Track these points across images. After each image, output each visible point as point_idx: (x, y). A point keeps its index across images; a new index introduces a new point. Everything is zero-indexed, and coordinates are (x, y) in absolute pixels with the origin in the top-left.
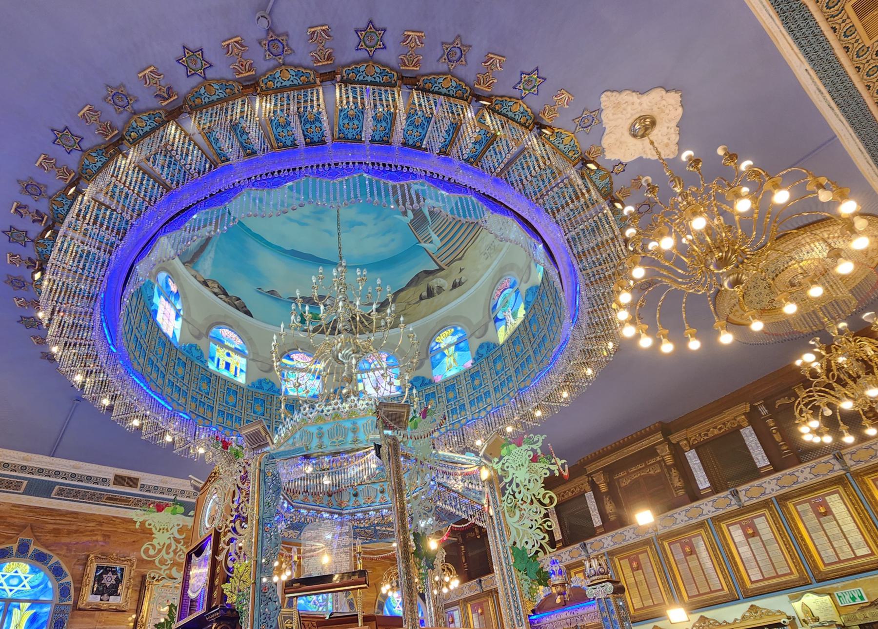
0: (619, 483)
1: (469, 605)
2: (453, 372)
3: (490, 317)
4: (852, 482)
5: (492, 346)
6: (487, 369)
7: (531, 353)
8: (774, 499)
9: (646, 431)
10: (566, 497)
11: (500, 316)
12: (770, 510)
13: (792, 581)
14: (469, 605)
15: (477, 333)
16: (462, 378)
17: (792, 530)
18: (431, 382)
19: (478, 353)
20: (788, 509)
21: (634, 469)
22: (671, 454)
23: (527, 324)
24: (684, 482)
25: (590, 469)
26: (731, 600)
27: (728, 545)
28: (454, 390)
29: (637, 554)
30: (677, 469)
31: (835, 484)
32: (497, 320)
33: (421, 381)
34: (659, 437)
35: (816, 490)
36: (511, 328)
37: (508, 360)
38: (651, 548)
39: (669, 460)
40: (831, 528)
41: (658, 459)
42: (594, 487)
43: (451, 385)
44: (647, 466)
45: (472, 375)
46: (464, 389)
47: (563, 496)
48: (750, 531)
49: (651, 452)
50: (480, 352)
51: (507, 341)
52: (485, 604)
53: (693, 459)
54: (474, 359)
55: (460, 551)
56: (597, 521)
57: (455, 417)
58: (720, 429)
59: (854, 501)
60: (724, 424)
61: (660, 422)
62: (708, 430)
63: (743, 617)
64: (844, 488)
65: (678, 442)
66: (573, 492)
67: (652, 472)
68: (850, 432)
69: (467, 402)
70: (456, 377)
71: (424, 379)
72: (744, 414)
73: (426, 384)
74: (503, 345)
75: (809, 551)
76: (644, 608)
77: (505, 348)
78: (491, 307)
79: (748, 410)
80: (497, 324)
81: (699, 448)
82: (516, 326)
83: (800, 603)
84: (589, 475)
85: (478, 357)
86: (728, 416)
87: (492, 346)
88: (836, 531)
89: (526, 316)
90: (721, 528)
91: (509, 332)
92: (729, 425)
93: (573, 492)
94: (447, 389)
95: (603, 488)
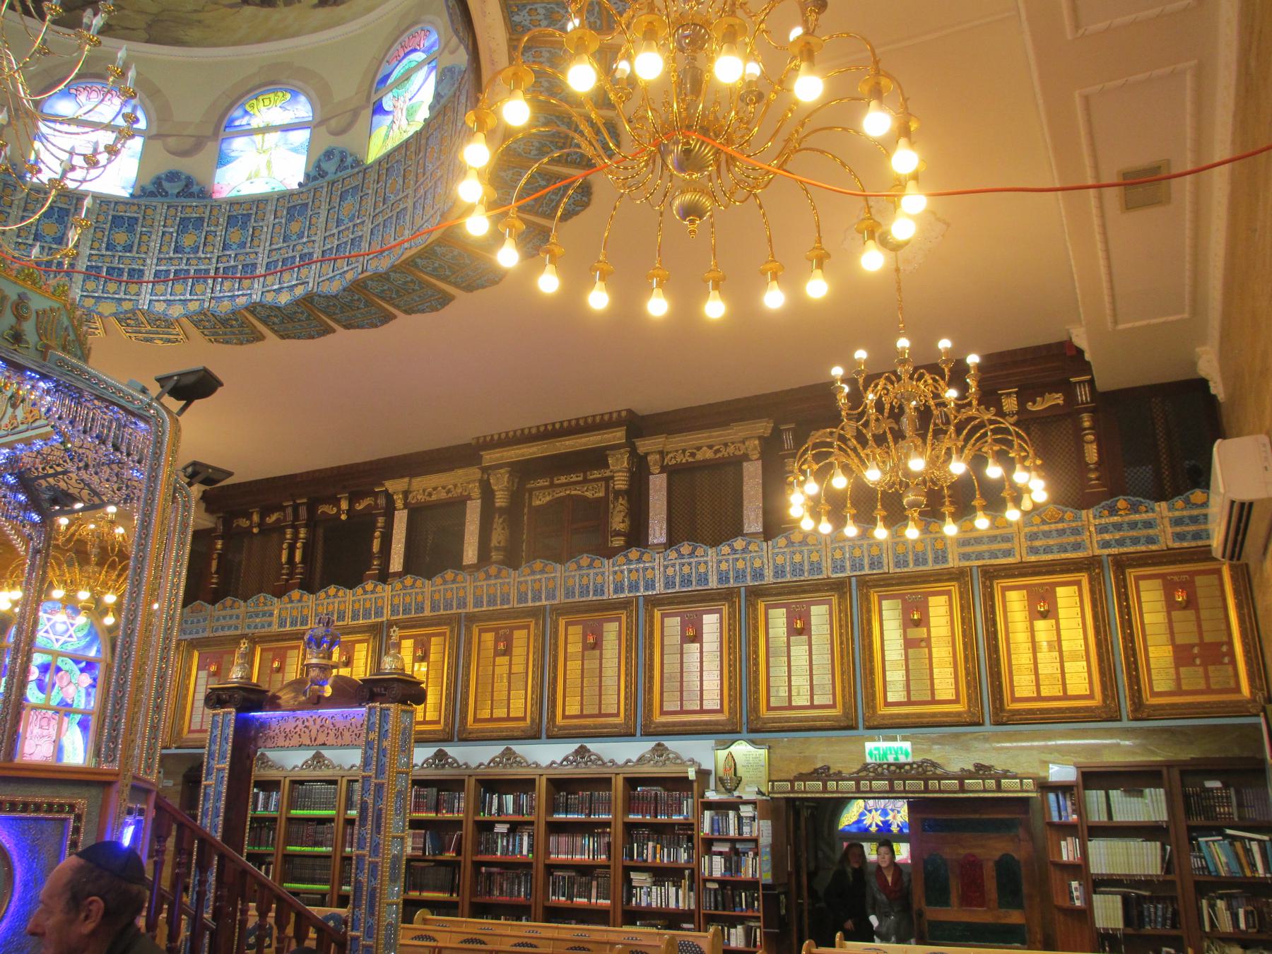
0: (530, 498)
1: (196, 654)
2: (259, 187)
3: (368, 98)
4: (854, 593)
5: (349, 160)
6: (325, 207)
7: (410, 203)
8: (743, 590)
9: (578, 423)
10: (434, 497)
11: (387, 104)
12: (732, 605)
13: (716, 723)
14: (196, 654)
15: (333, 123)
16: (270, 207)
17: (748, 644)
18: (204, 194)
19: (158, 182)
20: (755, 610)
21: (563, 480)
22: (629, 470)
23: (423, 142)
24: (631, 526)
25: (489, 457)
26: (626, 734)
27: (652, 646)
28: (244, 226)
29: (512, 629)
30: (629, 501)
31: (832, 589)
32: (379, 109)
33: (181, 184)
34: (618, 435)
35: (805, 592)
36: (397, 138)
37: (369, 202)
38: (536, 624)
39: (621, 483)
40: (799, 651)
41: (608, 474)
42: (487, 494)
43: (244, 212)
44: (585, 481)
45: (290, 206)
46: (265, 234)
47: (430, 495)
48: (691, 633)
49: (597, 458)
50: (325, 166)
51: (379, 162)
52: (226, 657)
53: (658, 485)
54: (307, 176)
55: (212, 548)
56: (470, 554)
57: (227, 284)
58: (718, 451)
59: (843, 623)
60: (726, 445)
61: (629, 411)
62: (699, 448)
63: (640, 759)
64: (840, 598)
65: (647, 454)
66: (449, 491)
67: (589, 494)
68: (857, 519)
69: (149, 275)
70: (258, 202)
71: (189, 182)
72: (760, 438)
73: (191, 195)
74: (371, 166)
75: (757, 684)
76: (491, 720)
77: (372, 176)
78: (379, 76)
79: (768, 433)
80: (377, 118)
81: (673, 473)
82: (406, 136)
83: (725, 752)
84: (485, 470)
85: (315, 174)
86: (736, 432)
87: (349, 160)
88: (804, 661)
89: (428, 123)
90: (652, 617)
91: (391, 145)
92: (731, 449)
93: (449, 491)
94: (231, 220)
95: (501, 500)
